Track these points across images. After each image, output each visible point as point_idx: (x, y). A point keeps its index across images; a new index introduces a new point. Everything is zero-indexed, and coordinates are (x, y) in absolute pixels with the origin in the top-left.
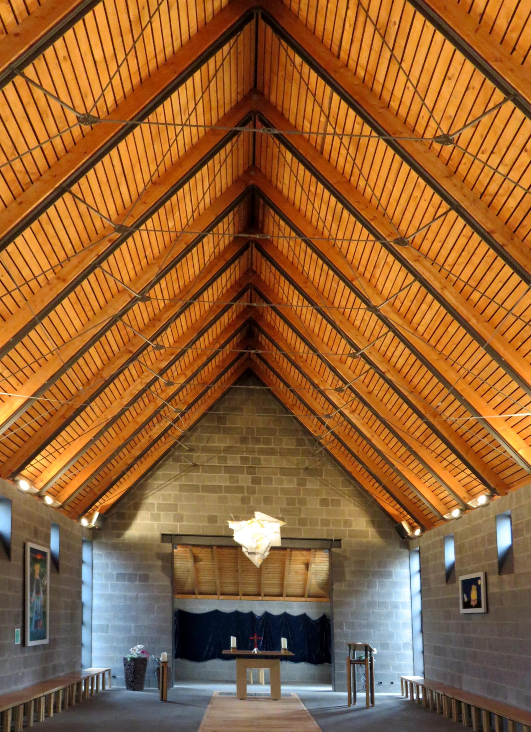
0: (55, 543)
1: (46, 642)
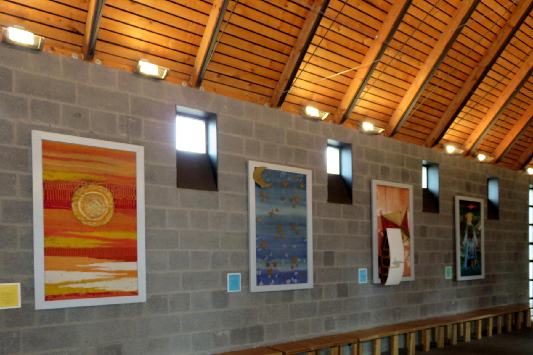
0: (493, 193)
1: (482, 277)
